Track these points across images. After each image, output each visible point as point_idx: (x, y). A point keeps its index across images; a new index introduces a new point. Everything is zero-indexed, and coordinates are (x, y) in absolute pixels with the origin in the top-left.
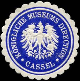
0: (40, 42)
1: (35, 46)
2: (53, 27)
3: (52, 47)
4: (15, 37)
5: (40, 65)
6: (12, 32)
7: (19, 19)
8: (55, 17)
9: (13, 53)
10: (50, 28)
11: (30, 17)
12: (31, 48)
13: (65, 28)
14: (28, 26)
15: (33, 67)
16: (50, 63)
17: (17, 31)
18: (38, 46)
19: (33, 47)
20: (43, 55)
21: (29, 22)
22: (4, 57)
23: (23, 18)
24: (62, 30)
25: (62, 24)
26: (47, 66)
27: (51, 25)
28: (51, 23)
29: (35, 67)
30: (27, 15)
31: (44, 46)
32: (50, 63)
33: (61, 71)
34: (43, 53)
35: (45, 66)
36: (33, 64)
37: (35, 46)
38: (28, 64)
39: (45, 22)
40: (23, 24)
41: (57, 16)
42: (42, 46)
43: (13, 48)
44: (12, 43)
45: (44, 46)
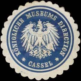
0: (40, 40)
1: (36, 44)
2: (54, 26)
3: (50, 47)
4: (15, 36)
5: (40, 64)
6: (12, 32)
7: (18, 20)
8: (52, 15)
9: (13, 52)
10: (49, 26)
11: (29, 16)
12: (32, 48)
13: (64, 26)
14: (26, 26)
15: (35, 65)
16: (49, 62)
17: (17, 31)
18: (38, 45)
19: (33, 46)
20: (42, 54)
21: (27, 23)
22: (66, 10)
23: (21, 19)
24: (61, 27)
25: (61, 22)
26: (46, 65)
27: (52, 24)
28: (52, 22)
29: (36, 65)
30: (26, 15)
31: (44, 44)
32: (49, 62)
33: (60, 71)
34: (43, 52)
35: (44, 65)
36: (34, 63)
37: (36, 44)
38: (30, 64)
39: (44, 20)
40: (21, 24)
41: (55, 14)
42: (42, 44)
43: (13, 47)
44: (13, 42)
45: (44, 44)
